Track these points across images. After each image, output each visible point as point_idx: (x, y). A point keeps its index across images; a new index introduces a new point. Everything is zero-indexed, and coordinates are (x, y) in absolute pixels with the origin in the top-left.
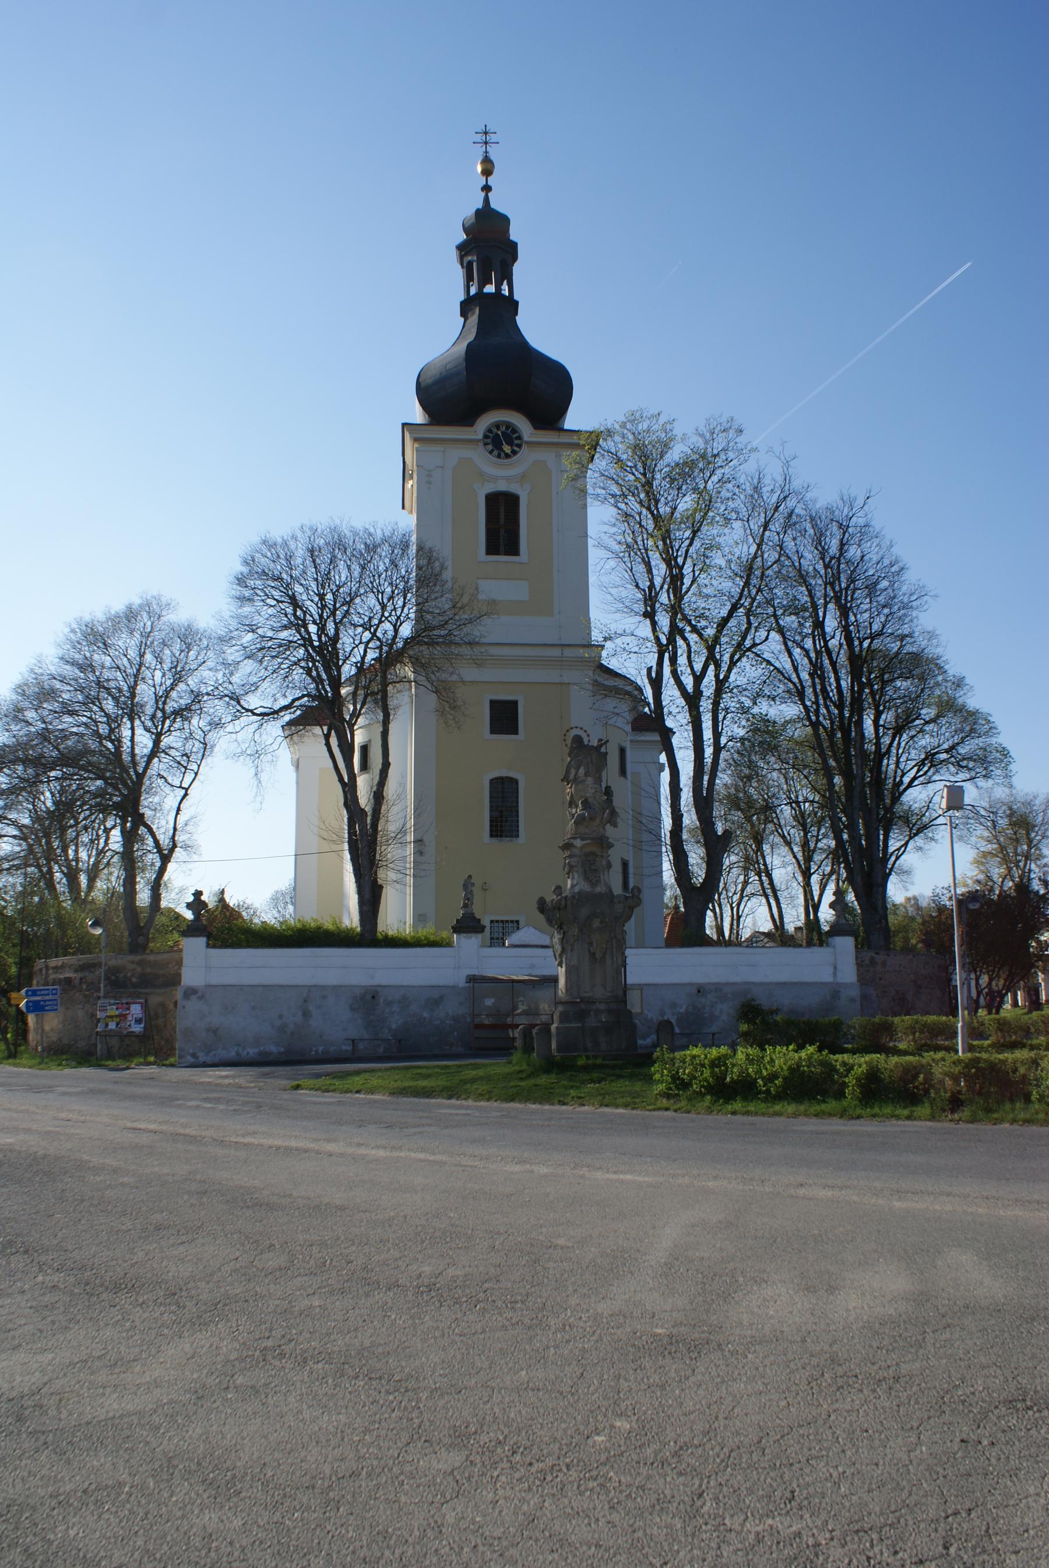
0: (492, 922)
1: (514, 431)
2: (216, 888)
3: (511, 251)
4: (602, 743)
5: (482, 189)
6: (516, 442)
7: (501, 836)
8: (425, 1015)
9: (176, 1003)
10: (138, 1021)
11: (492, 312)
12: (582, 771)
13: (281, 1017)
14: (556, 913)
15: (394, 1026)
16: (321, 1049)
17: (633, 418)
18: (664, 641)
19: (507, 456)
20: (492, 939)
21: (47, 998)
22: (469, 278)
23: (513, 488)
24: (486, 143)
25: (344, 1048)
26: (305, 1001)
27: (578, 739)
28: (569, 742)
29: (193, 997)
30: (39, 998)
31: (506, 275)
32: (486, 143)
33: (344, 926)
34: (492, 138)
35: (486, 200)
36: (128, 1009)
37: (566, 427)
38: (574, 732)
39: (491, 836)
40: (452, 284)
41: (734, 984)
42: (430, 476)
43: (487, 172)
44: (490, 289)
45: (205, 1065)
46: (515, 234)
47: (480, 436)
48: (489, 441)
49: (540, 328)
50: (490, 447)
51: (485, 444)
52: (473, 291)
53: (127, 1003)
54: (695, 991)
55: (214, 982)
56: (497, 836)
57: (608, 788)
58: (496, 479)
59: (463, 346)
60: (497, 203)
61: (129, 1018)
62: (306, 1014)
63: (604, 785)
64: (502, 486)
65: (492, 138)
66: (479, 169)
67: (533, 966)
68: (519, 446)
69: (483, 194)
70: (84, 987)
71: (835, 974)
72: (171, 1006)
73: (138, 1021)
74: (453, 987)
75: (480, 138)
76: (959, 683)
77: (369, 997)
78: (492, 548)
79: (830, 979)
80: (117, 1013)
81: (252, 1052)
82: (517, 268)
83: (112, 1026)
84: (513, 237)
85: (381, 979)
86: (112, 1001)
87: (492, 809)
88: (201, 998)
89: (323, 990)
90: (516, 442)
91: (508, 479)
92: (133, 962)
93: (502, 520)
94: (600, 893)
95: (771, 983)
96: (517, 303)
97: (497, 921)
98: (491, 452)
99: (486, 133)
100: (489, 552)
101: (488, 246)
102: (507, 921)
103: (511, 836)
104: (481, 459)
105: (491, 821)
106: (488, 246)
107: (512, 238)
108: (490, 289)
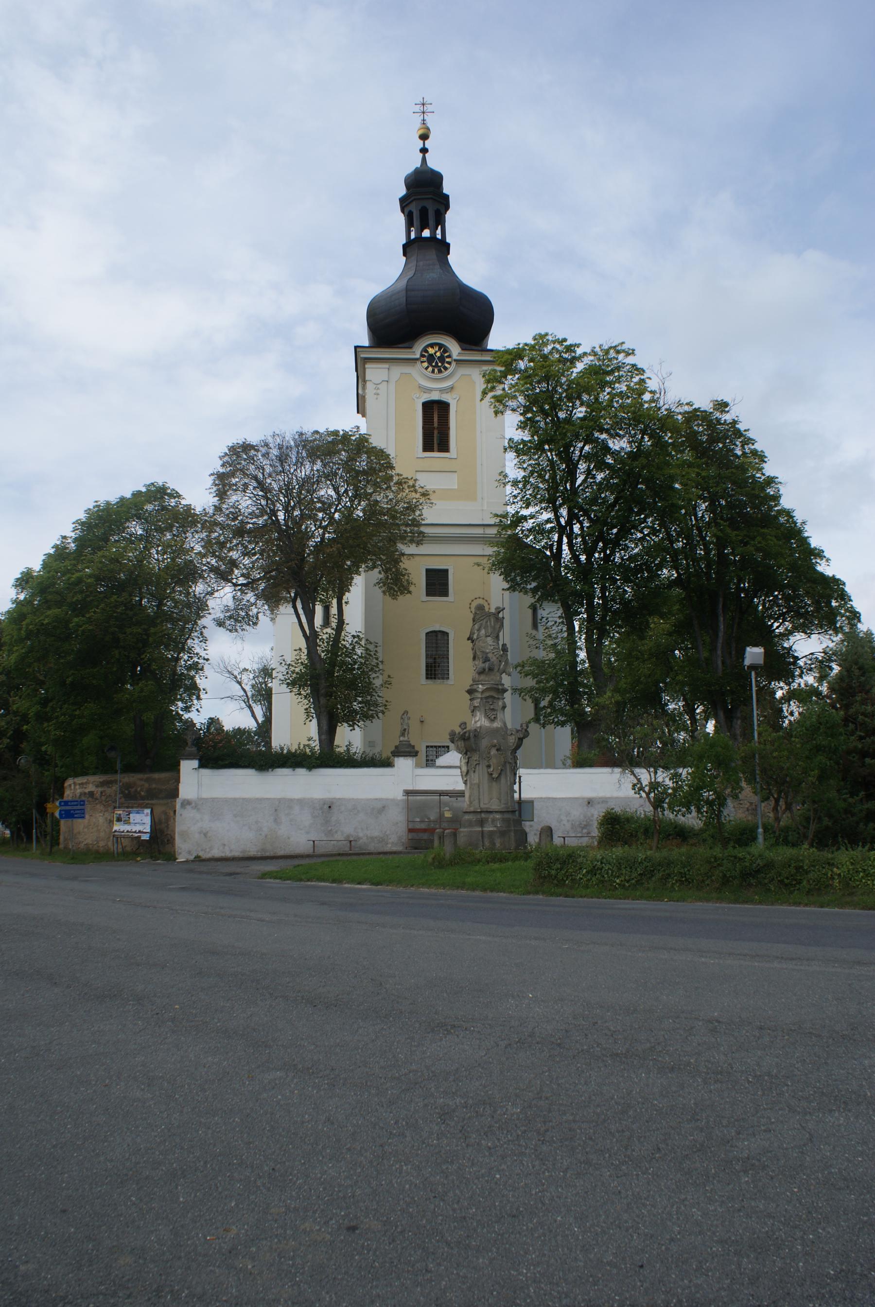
0: (427, 747)
2: (805, 518)
3: (444, 202)
4: (499, 610)
6: (447, 360)
7: (435, 678)
9: (175, 811)
12: (483, 632)
14: (467, 742)
17: (541, 339)
18: (563, 523)
20: (427, 760)
21: (75, 808)
22: (410, 223)
23: (445, 397)
24: (424, 113)
27: (480, 608)
28: (473, 610)
29: (188, 807)
31: (440, 220)
32: (424, 113)
34: (428, 108)
35: (424, 160)
37: (489, 347)
38: (480, 601)
39: (427, 678)
43: (424, 137)
44: (426, 233)
46: (447, 188)
47: (418, 356)
48: (425, 359)
49: (469, 265)
52: (413, 236)
56: (431, 678)
57: (504, 645)
58: (430, 390)
59: (404, 282)
63: (501, 643)
64: (435, 396)
65: (428, 108)
70: (103, 798)
72: (172, 813)
74: (393, 800)
75: (419, 108)
77: (326, 807)
78: (428, 447)
82: (449, 216)
84: (446, 191)
87: (427, 656)
90: (447, 360)
91: (442, 390)
92: (141, 779)
93: (436, 425)
94: (497, 727)
96: (448, 245)
97: (432, 747)
99: (423, 104)
100: (426, 449)
101: (425, 199)
102: (440, 747)
103: (443, 678)
105: (427, 666)
106: (425, 199)
107: (445, 191)
108: (426, 233)
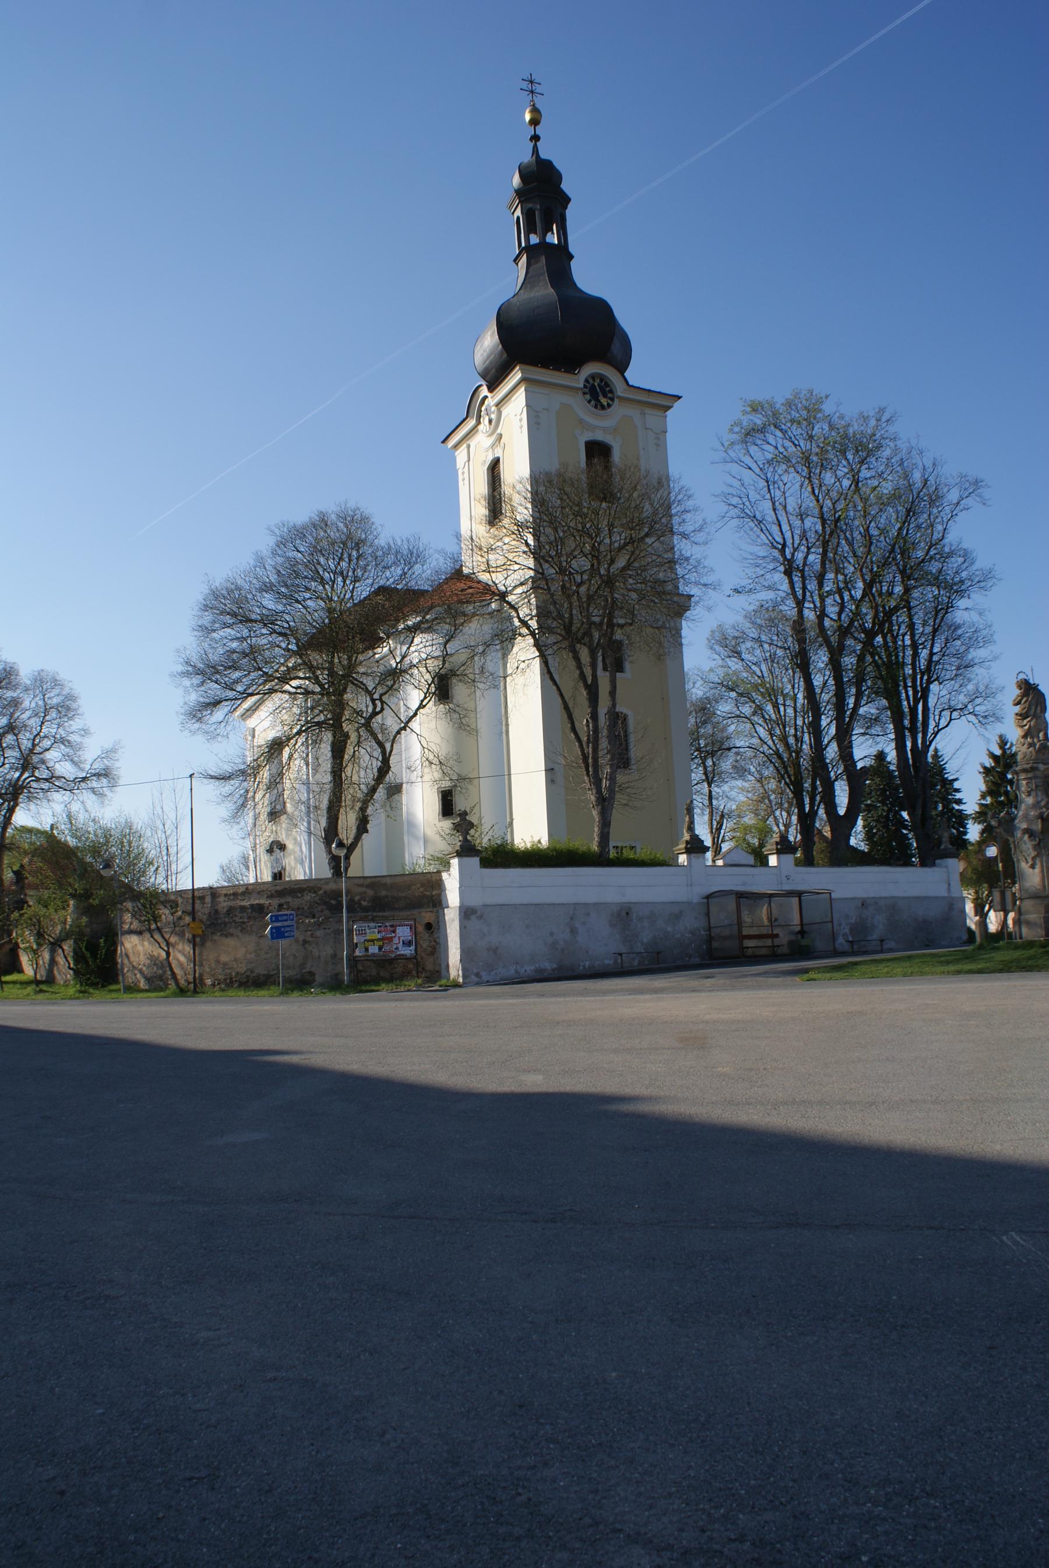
1: (607, 385)
5: (531, 139)
8: (669, 929)
10: (408, 944)
11: (552, 261)
13: (552, 934)
15: (645, 940)
16: (587, 963)
19: (603, 408)
21: (286, 923)
23: (607, 439)
25: (606, 962)
26: (572, 918)
29: (473, 917)
30: (280, 924)
32: (532, 92)
33: (408, 869)
36: (394, 932)
40: (504, 225)
41: (886, 898)
42: (538, 417)
45: (488, 983)
47: (582, 386)
50: (588, 397)
51: (584, 394)
53: (392, 926)
54: (860, 905)
55: (489, 901)
60: (543, 155)
61: (396, 941)
62: (573, 931)
64: (599, 436)
65: (538, 89)
66: (528, 117)
67: (745, 884)
68: (612, 399)
69: (532, 144)
71: (949, 889)
73: (408, 944)
74: (689, 903)
75: (525, 85)
76: (85, 732)
77: (624, 914)
79: (945, 894)
80: (379, 936)
81: (529, 969)
83: (374, 949)
85: (632, 896)
86: (372, 925)
88: (480, 917)
89: (587, 908)
91: (604, 429)
95: (908, 898)
98: (589, 402)
101: (542, 193)
104: (579, 405)
106: (542, 193)
